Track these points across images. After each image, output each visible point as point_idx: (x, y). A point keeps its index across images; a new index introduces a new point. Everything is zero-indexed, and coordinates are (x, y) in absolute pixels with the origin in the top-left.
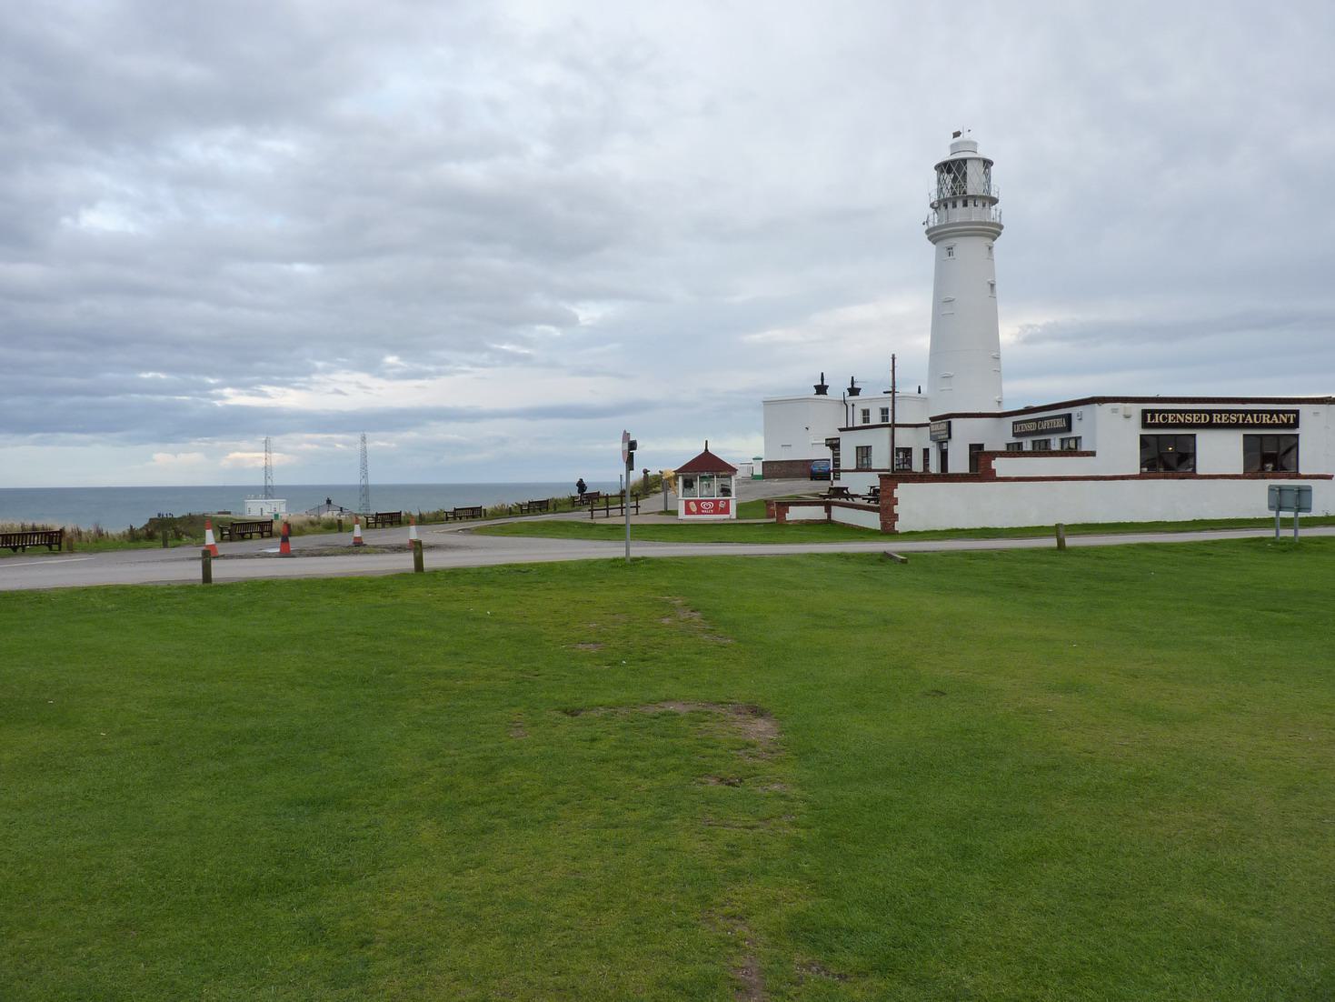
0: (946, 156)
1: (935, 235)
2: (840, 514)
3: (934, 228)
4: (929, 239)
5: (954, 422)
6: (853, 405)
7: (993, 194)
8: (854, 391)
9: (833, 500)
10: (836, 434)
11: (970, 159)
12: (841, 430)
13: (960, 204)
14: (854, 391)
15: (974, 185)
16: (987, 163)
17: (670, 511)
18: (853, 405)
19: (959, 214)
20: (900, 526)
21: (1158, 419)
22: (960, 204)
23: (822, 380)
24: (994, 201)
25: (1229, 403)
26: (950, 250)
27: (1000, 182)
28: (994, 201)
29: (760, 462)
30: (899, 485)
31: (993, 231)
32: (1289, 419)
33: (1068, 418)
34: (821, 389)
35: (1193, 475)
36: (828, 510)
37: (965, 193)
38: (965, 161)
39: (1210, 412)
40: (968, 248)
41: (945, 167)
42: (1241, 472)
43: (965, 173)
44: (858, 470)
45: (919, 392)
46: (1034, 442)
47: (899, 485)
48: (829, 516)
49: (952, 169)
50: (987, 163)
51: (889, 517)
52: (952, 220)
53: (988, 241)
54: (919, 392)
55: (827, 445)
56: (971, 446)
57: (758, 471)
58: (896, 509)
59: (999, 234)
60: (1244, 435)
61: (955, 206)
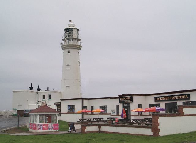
0: (67, 27)
1: (64, 48)
2: (104, 129)
3: (64, 45)
4: (62, 49)
5: (134, 97)
6: (40, 94)
7: (79, 38)
8: (39, 90)
9: (126, 124)
10: (59, 101)
11: (75, 28)
12: (61, 100)
13: (71, 40)
14: (39, 90)
15: (75, 36)
16: (78, 30)
17: (21, 128)
18: (40, 94)
19: (72, 42)
20: (161, 134)
21: (158, 99)
22: (71, 40)
23: (32, 85)
24: (79, 40)
25: (171, 93)
26: (69, 52)
27: (81, 35)
28: (79, 40)
29: (16, 110)
30: (160, 118)
31: (79, 48)
32: (157, 99)
33: (188, 95)
34: (31, 88)
35: (74, 113)
36: (100, 128)
37: (73, 37)
38: (73, 28)
39: (170, 96)
40: (73, 51)
41: (66, 30)
42: (67, 112)
43: (73, 32)
44: (69, 113)
45: (54, 90)
46: (183, 103)
47: (160, 118)
48: (100, 130)
49: (69, 31)
50: (78, 30)
51: (156, 130)
52: (70, 44)
53: (78, 50)
54: (54, 90)
55: (55, 105)
56: (91, 107)
57: (15, 113)
58: (159, 127)
59: (81, 49)
60: (166, 103)
61: (70, 40)
